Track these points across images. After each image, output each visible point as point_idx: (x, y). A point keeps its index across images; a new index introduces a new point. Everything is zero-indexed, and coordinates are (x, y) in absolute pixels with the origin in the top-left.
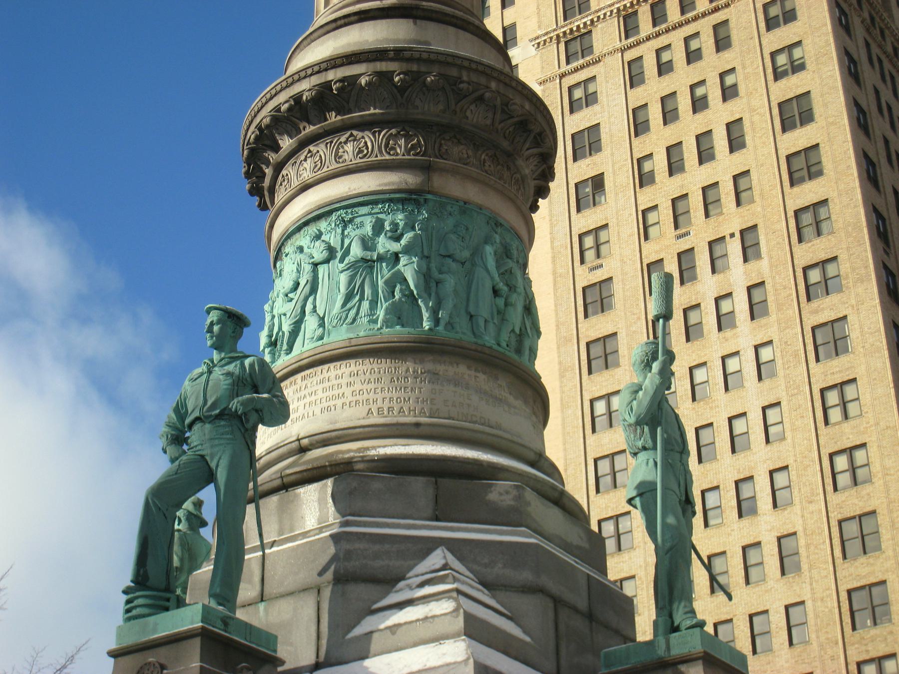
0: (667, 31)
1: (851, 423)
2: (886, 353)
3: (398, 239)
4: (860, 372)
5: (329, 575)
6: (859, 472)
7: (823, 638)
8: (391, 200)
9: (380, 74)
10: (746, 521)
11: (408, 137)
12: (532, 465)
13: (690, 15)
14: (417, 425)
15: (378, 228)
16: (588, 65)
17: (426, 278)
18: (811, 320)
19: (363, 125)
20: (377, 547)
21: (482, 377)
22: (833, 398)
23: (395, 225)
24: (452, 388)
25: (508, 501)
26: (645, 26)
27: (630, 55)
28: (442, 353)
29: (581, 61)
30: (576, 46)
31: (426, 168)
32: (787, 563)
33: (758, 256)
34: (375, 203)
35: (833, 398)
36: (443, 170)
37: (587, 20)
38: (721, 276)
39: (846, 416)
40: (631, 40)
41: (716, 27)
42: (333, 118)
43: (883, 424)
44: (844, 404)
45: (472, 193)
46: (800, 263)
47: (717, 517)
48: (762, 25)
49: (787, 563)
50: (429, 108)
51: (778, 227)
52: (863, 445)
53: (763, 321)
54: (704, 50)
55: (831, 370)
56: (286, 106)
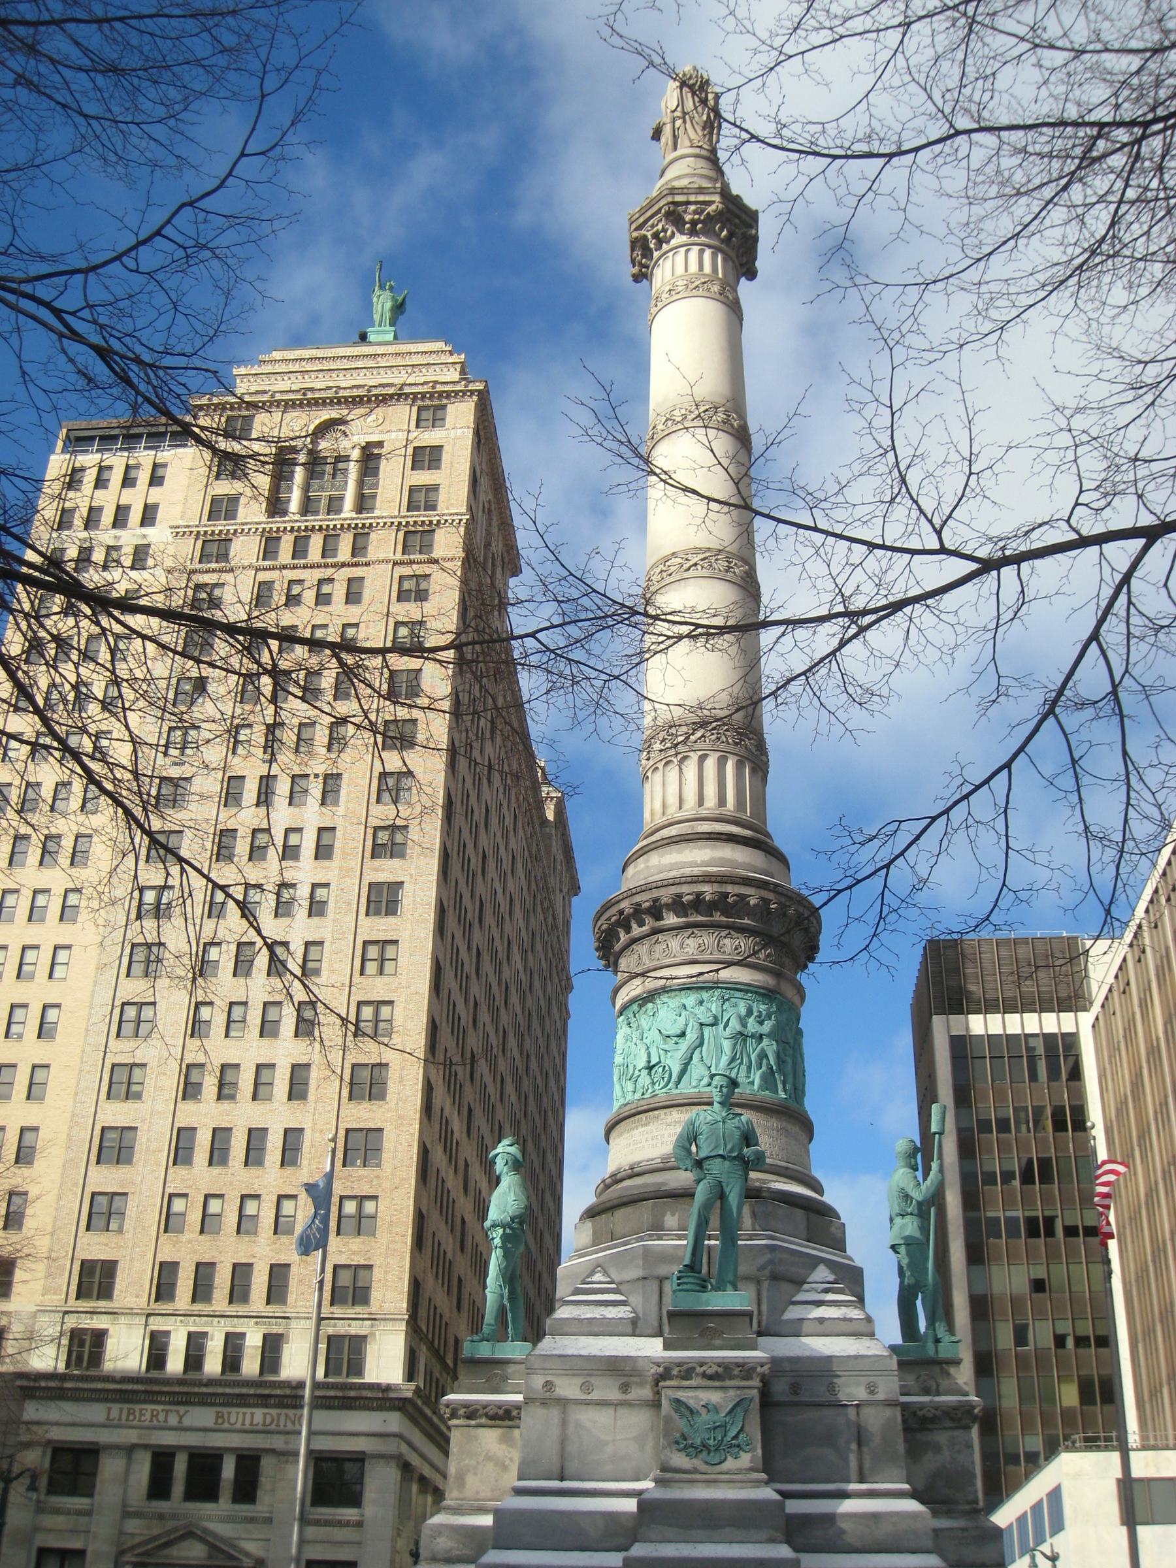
0: (305, 567)
1: (386, 979)
2: (432, 926)
3: (761, 1023)
4: (404, 937)
5: (767, 1272)
6: (382, 1025)
7: (314, 1167)
9: (763, 899)
10: (265, 1042)
13: (330, 560)
15: (750, 1012)
16: (221, 571)
18: (370, 877)
22: (373, 952)
26: (285, 554)
27: (263, 576)
29: (214, 565)
30: (213, 549)
31: (778, 975)
32: (297, 1090)
33: (336, 803)
34: (746, 992)
35: (373, 952)
37: (232, 528)
38: (296, 810)
39: (381, 972)
40: (267, 563)
41: (350, 580)
42: (718, 917)
43: (413, 989)
44: (382, 960)
46: (374, 822)
47: (237, 1030)
48: (394, 594)
49: (297, 1090)
50: (777, 929)
51: (361, 782)
52: (391, 1003)
53: (326, 863)
54: (334, 597)
55: (379, 927)
56: (690, 897)
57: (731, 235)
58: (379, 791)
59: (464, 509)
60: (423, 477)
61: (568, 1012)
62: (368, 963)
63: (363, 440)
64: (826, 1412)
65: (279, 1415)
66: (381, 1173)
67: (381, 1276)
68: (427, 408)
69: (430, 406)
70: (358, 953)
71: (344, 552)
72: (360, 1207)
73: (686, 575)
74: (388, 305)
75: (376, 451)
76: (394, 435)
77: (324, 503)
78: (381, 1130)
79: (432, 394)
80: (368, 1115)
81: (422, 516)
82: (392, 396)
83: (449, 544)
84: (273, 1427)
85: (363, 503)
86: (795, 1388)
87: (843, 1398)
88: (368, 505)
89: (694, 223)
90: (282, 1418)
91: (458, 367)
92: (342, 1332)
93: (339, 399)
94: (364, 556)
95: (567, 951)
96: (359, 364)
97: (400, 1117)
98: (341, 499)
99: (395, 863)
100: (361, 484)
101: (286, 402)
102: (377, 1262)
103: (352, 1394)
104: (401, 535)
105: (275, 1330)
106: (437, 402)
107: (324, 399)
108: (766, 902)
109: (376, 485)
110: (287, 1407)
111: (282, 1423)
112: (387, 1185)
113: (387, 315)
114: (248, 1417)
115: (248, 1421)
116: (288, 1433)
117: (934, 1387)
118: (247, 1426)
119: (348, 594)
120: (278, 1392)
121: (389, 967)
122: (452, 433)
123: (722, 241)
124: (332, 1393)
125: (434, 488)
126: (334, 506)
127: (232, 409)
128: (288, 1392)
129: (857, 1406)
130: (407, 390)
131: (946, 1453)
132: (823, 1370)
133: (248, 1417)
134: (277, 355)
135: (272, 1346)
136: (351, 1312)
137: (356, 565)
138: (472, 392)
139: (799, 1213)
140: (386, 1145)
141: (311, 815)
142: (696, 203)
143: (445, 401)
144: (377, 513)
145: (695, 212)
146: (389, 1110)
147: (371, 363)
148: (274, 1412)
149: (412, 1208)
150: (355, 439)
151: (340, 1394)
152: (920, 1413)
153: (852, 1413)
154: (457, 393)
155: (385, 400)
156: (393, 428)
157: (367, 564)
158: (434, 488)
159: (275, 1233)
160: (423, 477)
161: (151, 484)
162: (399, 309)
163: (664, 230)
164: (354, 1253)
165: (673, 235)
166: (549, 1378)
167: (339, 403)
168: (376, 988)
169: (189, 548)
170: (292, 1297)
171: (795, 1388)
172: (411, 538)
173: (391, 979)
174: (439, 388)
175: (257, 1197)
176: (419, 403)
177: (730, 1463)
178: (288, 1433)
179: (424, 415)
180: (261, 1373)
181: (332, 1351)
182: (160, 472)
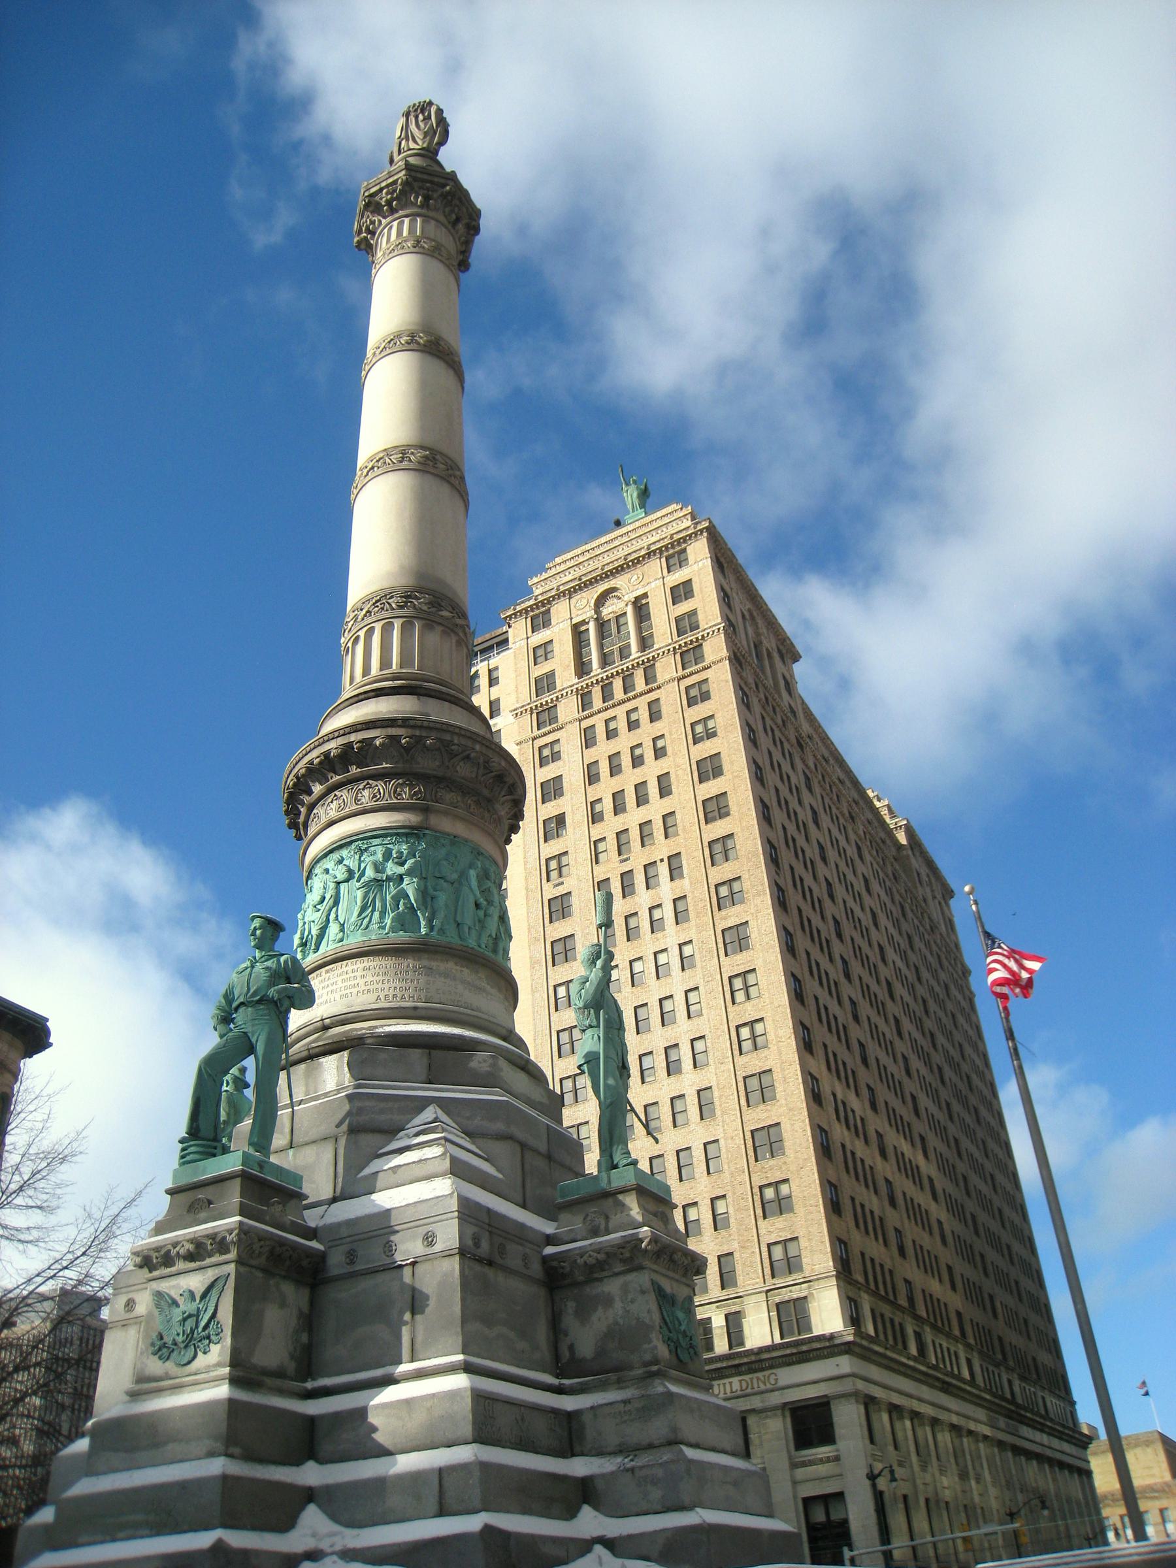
0: (614, 706)
1: (752, 1002)
4: (758, 964)
5: (345, 1127)
7: (733, 1169)
8: (397, 834)
9: (391, 737)
11: (411, 787)
12: (504, 1039)
13: (631, 694)
14: (415, 1008)
15: (387, 855)
17: (425, 895)
19: (376, 776)
20: (382, 1105)
21: (466, 971)
22: (738, 984)
23: (400, 853)
24: (443, 979)
25: (485, 1068)
26: (598, 703)
27: (585, 724)
28: (436, 952)
29: (548, 728)
31: (425, 810)
32: (705, 1108)
33: (681, 876)
34: (385, 836)
35: (738, 984)
36: (438, 812)
39: (748, 998)
43: (776, 1004)
44: (746, 988)
45: (459, 829)
46: (713, 882)
48: (685, 702)
51: (695, 854)
52: (761, 1020)
53: (685, 925)
54: (641, 721)
55: (737, 963)
57: (427, 198)
58: (712, 856)
59: (719, 620)
60: (684, 607)
61: (971, 992)
62: (736, 994)
63: (631, 597)
64: (381, 1278)
65: (751, 1379)
66: (788, 1160)
67: (807, 1244)
68: (672, 556)
69: (674, 554)
70: (727, 988)
71: (640, 684)
72: (777, 1192)
73: (368, 478)
74: (635, 495)
75: (644, 602)
76: (653, 585)
77: (616, 654)
78: (778, 1124)
79: (672, 543)
80: (766, 1115)
81: (690, 637)
82: (644, 557)
83: (716, 649)
84: (749, 1390)
85: (645, 643)
86: (352, 1256)
87: (399, 1258)
88: (649, 643)
89: (389, 203)
90: (755, 1381)
91: (689, 517)
92: (787, 1298)
93: (606, 573)
94: (656, 681)
95: (957, 946)
96: (617, 543)
97: (790, 1110)
98: (629, 646)
99: (738, 908)
100: (639, 630)
101: (569, 590)
102: (801, 1233)
103: (804, 1348)
104: (678, 656)
105: (733, 1309)
106: (677, 549)
107: (595, 578)
108: (394, 739)
109: (651, 627)
110: (755, 1371)
111: (756, 1385)
112: (793, 1168)
113: (636, 502)
114: (728, 1387)
115: (728, 1390)
116: (762, 1392)
117: (603, 1227)
118: (729, 1394)
119: (651, 715)
120: (745, 1360)
121: (753, 991)
122: (695, 567)
123: (422, 206)
124: (788, 1351)
125: (693, 613)
126: (624, 652)
127: (532, 610)
128: (753, 1358)
129: (413, 1264)
130: (653, 548)
131: (618, 1305)
132: (381, 1227)
133: (728, 1387)
134: (558, 560)
135: (734, 1322)
136: (789, 1280)
137: (650, 691)
138: (701, 531)
139: (416, 1054)
140: (786, 1135)
141: (666, 890)
142: (387, 186)
143: (684, 546)
144: (656, 647)
145: (387, 194)
146: (781, 1106)
147: (625, 539)
148: (747, 1377)
149: (818, 1182)
150: (626, 598)
151: (795, 1351)
152: (580, 1261)
153: (407, 1272)
154: (690, 536)
155: (637, 562)
156: (653, 581)
157: (659, 688)
158: (693, 613)
159: (716, 1230)
160: (684, 607)
161: (490, 686)
162: (644, 495)
163: (373, 222)
164: (781, 1230)
165: (380, 222)
166: (131, 1296)
167: (607, 576)
168: (748, 1011)
169: (528, 721)
170: (740, 1279)
171: (352, 1256)
172: (686, 657)
173: (757, 1001)
174: (676, 537)
175: (695, 1204)
176: (665, 554)
177: (202, 1361)
178: (762, 1392)
179: (672, 562)
180: (731, 1348)
181: (782, 1313)
182: (495, 675)
